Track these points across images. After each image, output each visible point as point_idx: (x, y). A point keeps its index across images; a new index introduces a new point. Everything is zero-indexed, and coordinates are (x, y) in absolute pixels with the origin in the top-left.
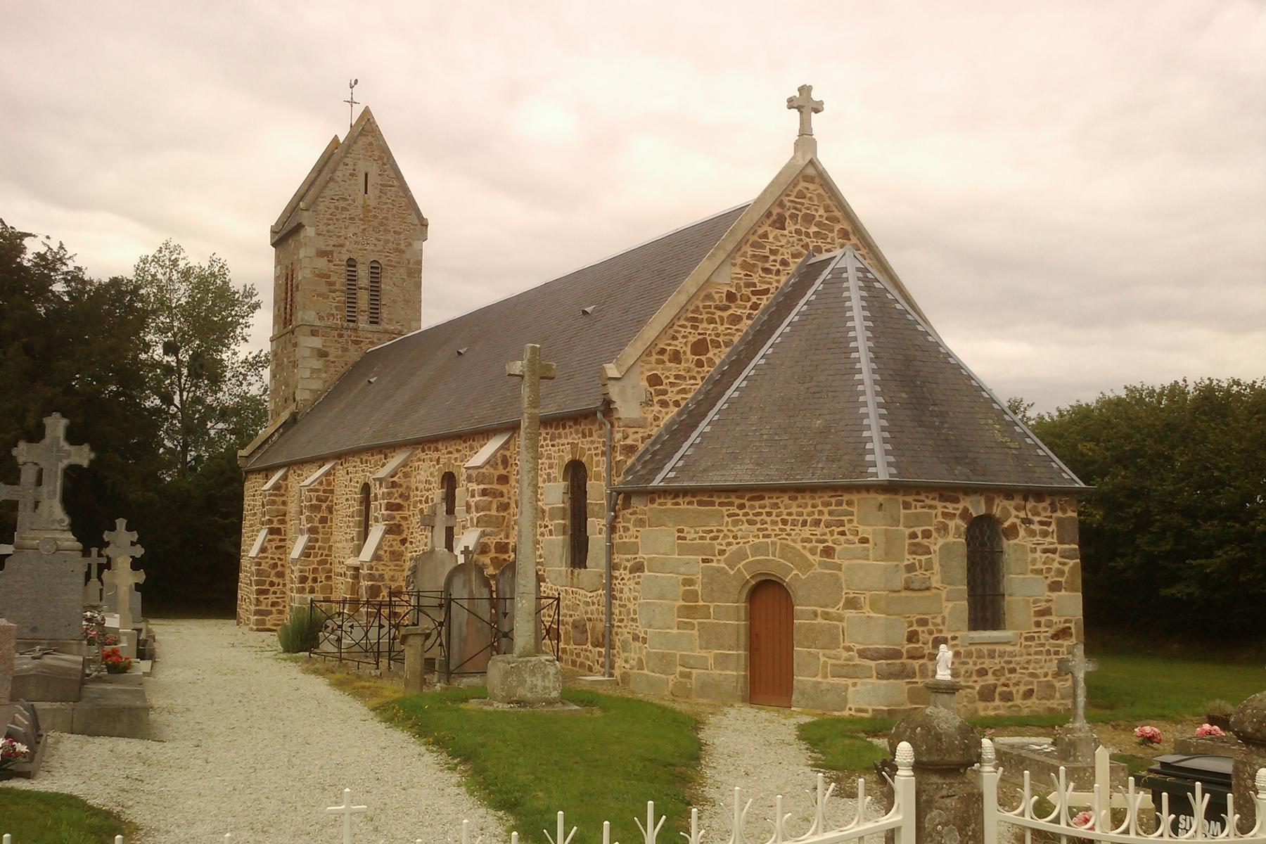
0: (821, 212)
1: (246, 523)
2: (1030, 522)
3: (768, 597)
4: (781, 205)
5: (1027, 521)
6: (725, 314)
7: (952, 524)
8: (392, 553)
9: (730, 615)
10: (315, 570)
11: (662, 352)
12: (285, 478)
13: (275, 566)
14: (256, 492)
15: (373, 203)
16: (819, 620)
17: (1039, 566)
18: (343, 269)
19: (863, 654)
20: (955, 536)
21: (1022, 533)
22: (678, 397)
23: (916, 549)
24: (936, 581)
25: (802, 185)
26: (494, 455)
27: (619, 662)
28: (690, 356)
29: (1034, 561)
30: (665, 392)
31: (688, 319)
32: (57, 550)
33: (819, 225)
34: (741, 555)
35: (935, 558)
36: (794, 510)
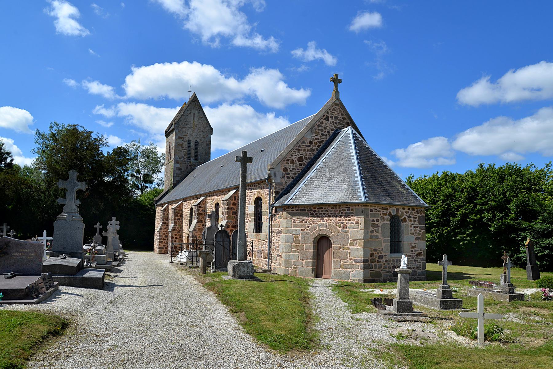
0: (341, 116)
1: (156, 221)
2: (410, 217)
3: (322, 243)
4: (328, 113)
5: (409, 217)
6: (309, 148)
7: (385, 217)
8: (199, 229)
9: (309, 249)
10: (176, 235)
11: (288, 160)
12: (168, 206)
13: (164, 234)
14: (159, 211)
15: (196, 123)
16: (341, 250)
17: (413, 232)
18: (187, 143)
19: (355, 261)
20: (386, 222)
21: (407, 220)
22: (293, 176)
23: (374, 226)
24: (380, 236)
25: (335, 106)
26: (231, 196)
27: (273, 264)
28: (297, 162)
29: (411, 230)
30: (289, 174)
31: (296, 149)
32: (73, 220)
33: (339, 120)
34: (314, 228)
35: (380, 229)
36: (333, 212)
